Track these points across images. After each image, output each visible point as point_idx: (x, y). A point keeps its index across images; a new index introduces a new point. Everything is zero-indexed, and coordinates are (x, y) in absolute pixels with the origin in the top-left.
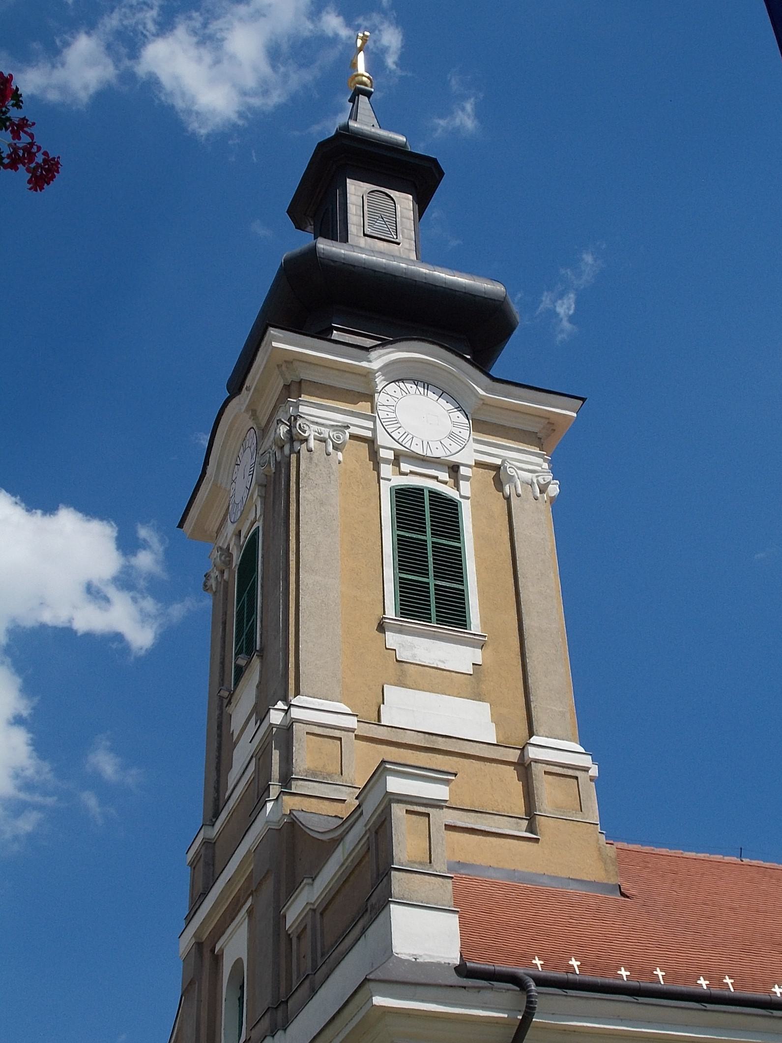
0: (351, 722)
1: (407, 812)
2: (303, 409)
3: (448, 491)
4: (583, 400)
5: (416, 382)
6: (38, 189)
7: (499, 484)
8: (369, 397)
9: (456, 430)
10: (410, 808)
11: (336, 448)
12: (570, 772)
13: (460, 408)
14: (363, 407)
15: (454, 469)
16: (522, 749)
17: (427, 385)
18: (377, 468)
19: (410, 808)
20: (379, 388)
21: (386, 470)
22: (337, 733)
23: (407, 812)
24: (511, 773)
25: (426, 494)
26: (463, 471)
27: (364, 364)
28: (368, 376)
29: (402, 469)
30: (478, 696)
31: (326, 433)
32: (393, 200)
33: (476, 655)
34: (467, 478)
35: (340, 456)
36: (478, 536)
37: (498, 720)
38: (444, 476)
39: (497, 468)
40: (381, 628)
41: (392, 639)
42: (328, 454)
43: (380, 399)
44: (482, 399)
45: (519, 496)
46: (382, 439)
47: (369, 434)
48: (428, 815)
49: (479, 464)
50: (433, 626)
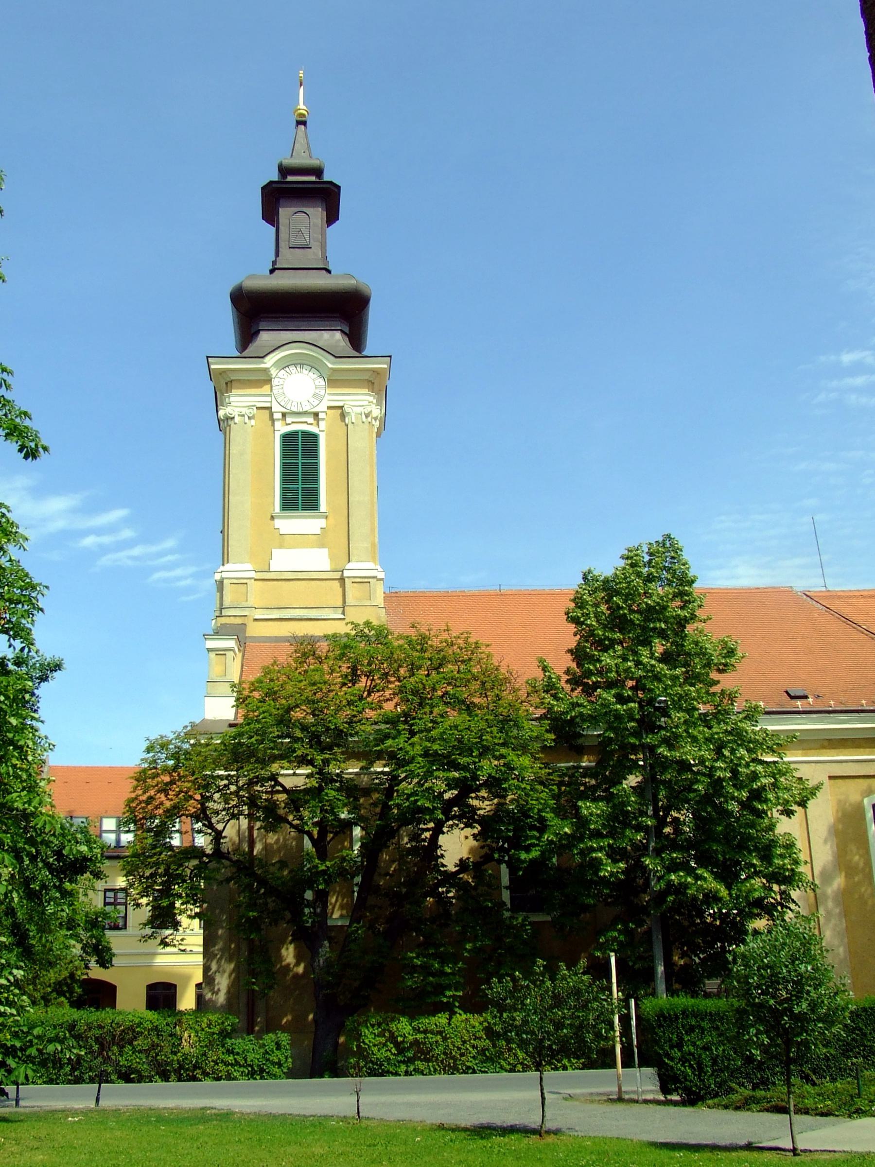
0: (253, 575)
1: (216, 654)
2: (232, 399)
3: (313, 429)
4: (390, 357)
5: (295, 365)
6: (24, 452)
7: (343, 416)
8: (269, 381)
9: (317, 391)
10: (217, 653)
11: (249, 418)
12: (366, 580)
13: (321, 376)
14: (266, 389)
15: (316, 415)
16: (342, 571)
17: (302, 365)
18: (273, 425)
19: (217, 653)
20: (273, 376)
21: (278, 425)
22: (245, 581)
23: (216, 654)
24: (337, 584)
25: (300, 434)
26: (321, 416)
27: (262, 366)
28: (266, 371)
29: (288, 422)
30: (322, 546)
31: (244, 411)
32: (306, 213)
33: (323, 523)
34: (323, 419)
35: (253, 422)
36: (329, 453)
37: (332, 557)
38: (311, 420)
39: (341, 407)
40: (272, 518)
41: (278, 523)
42: (245, 423)
43: (275, 382)
44: (332, 369)
45: (353, 423)
46: (276, 408)
47: (268, 405)
48: (225, 654)
49: (329, 408)
50: (301, 513)
